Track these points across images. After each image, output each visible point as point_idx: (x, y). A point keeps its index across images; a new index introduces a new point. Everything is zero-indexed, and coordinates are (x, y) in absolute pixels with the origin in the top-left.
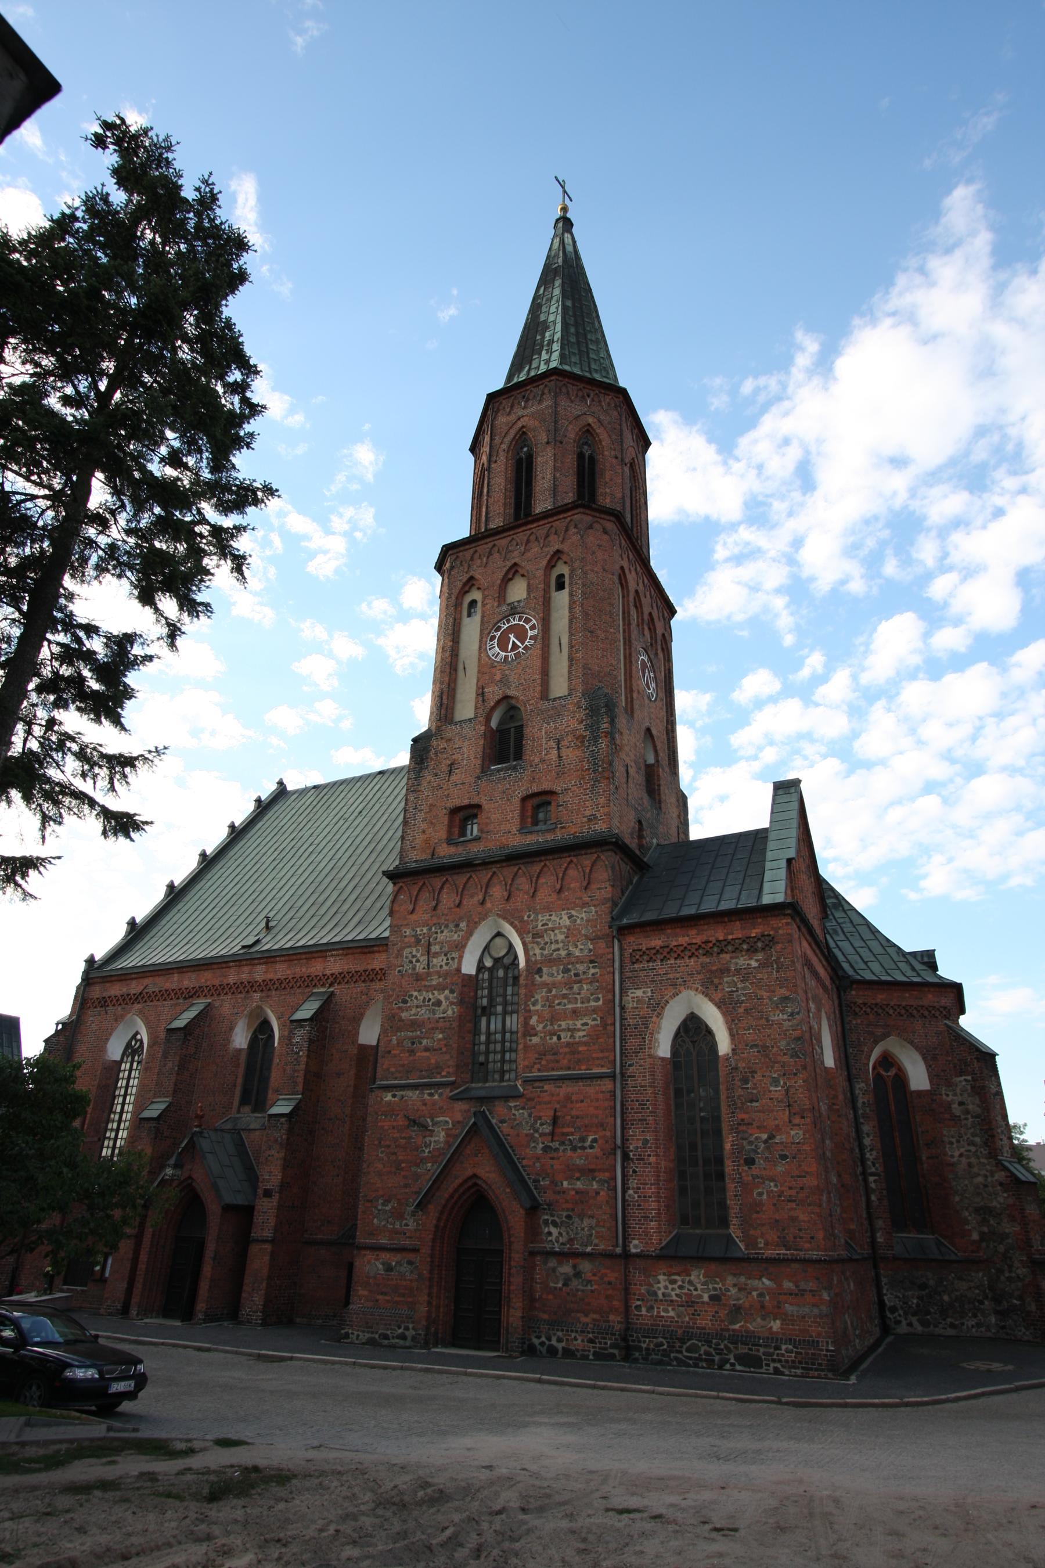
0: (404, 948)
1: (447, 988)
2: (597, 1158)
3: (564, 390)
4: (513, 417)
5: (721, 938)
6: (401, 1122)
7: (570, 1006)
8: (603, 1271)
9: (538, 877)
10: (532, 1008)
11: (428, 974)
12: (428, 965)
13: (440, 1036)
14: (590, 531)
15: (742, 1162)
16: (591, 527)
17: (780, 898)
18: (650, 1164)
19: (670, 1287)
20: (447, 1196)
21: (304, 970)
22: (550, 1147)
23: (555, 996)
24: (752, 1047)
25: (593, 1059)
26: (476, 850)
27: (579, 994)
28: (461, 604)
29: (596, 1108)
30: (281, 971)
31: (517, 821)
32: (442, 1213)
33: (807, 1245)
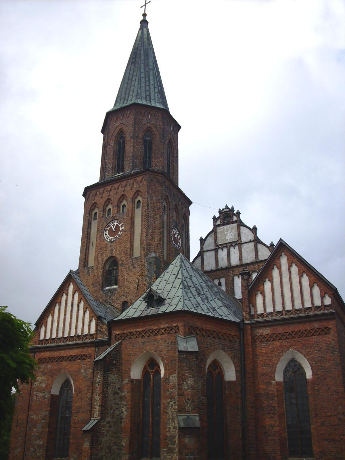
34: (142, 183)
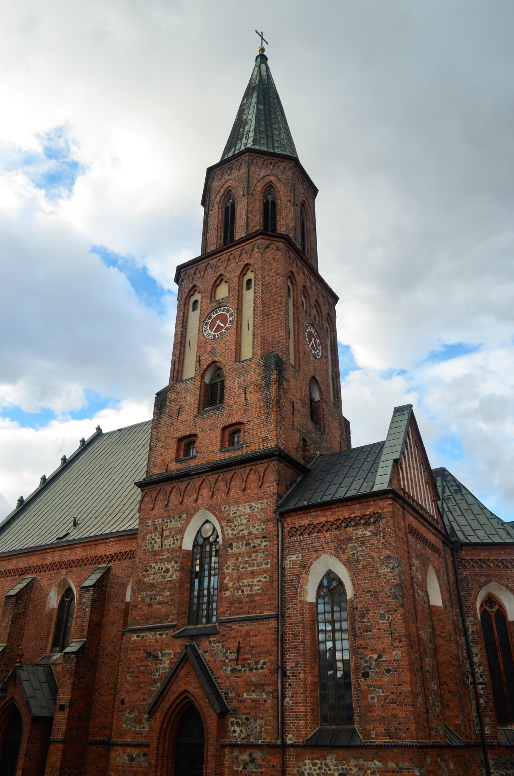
0: (147, 534)
1: (173, 560)
2: (266, 676)
3: (254, 161)
4: (223, 181)
5: (347, 517)
6: (142, 654)
7: (250, 569)
8: (269, 758)
9: (231, 481)
10: (226, 571)
11: (162, 551)
12: (162, 545)
13: (168, 593)
14: (268, 250)
15: (361, 675)
16: (268, 247)
17: (385, 487)
18: (300, 679)
19: (313, 768)
20: (168, 706)
21: (93, 552)
22: (236, 669)
23: (241, 562)
24: (367, 592)
25: (264, 605)
26: (193, 464)
27: (256, 560)
28: (189, 303)
29: (266, 640)
30: (78, 554)
31: (219, 444)
32: (164, 718)
33: (404, 735)
34: (255, 254)
